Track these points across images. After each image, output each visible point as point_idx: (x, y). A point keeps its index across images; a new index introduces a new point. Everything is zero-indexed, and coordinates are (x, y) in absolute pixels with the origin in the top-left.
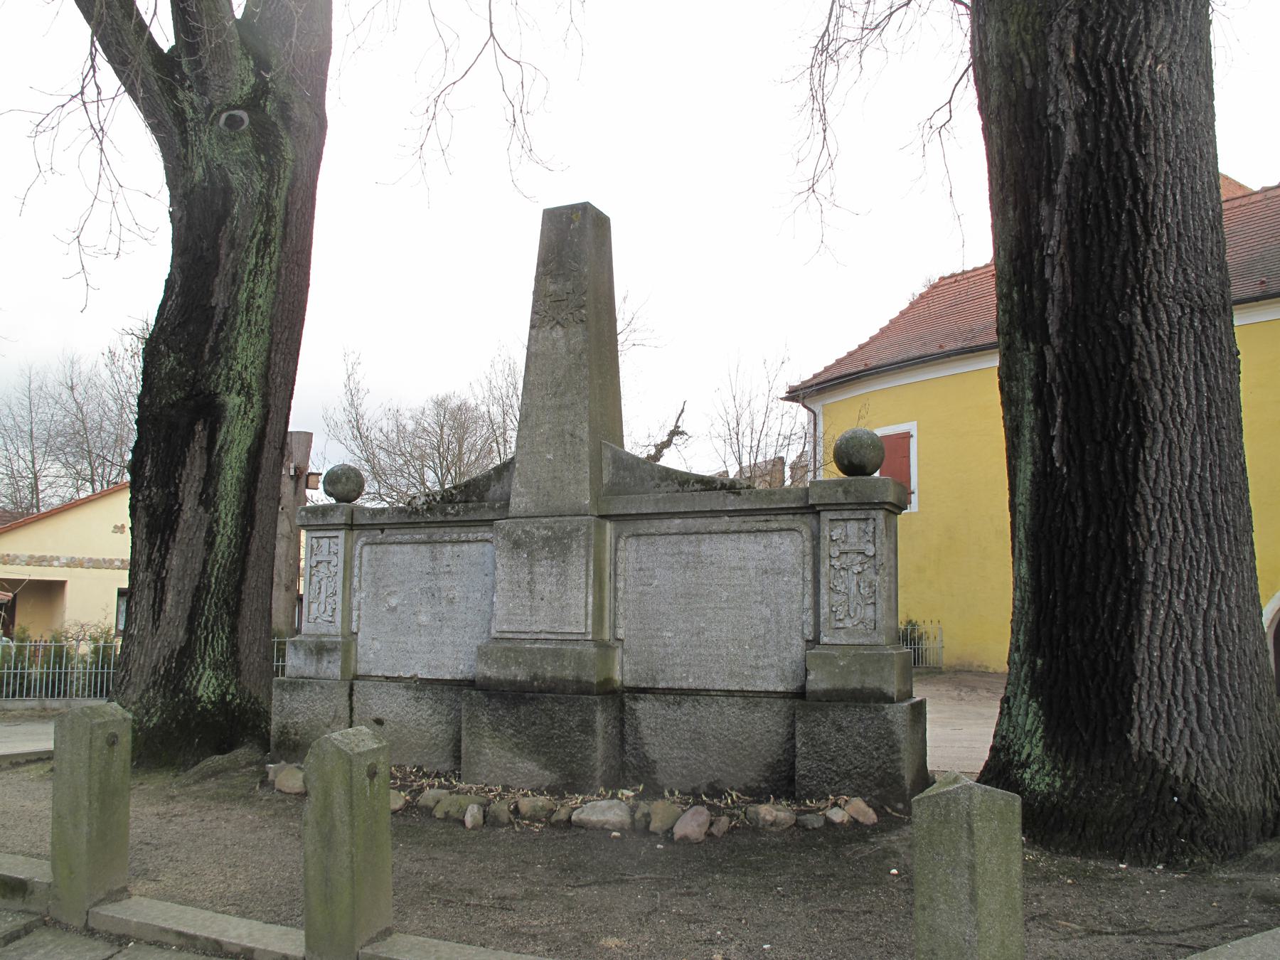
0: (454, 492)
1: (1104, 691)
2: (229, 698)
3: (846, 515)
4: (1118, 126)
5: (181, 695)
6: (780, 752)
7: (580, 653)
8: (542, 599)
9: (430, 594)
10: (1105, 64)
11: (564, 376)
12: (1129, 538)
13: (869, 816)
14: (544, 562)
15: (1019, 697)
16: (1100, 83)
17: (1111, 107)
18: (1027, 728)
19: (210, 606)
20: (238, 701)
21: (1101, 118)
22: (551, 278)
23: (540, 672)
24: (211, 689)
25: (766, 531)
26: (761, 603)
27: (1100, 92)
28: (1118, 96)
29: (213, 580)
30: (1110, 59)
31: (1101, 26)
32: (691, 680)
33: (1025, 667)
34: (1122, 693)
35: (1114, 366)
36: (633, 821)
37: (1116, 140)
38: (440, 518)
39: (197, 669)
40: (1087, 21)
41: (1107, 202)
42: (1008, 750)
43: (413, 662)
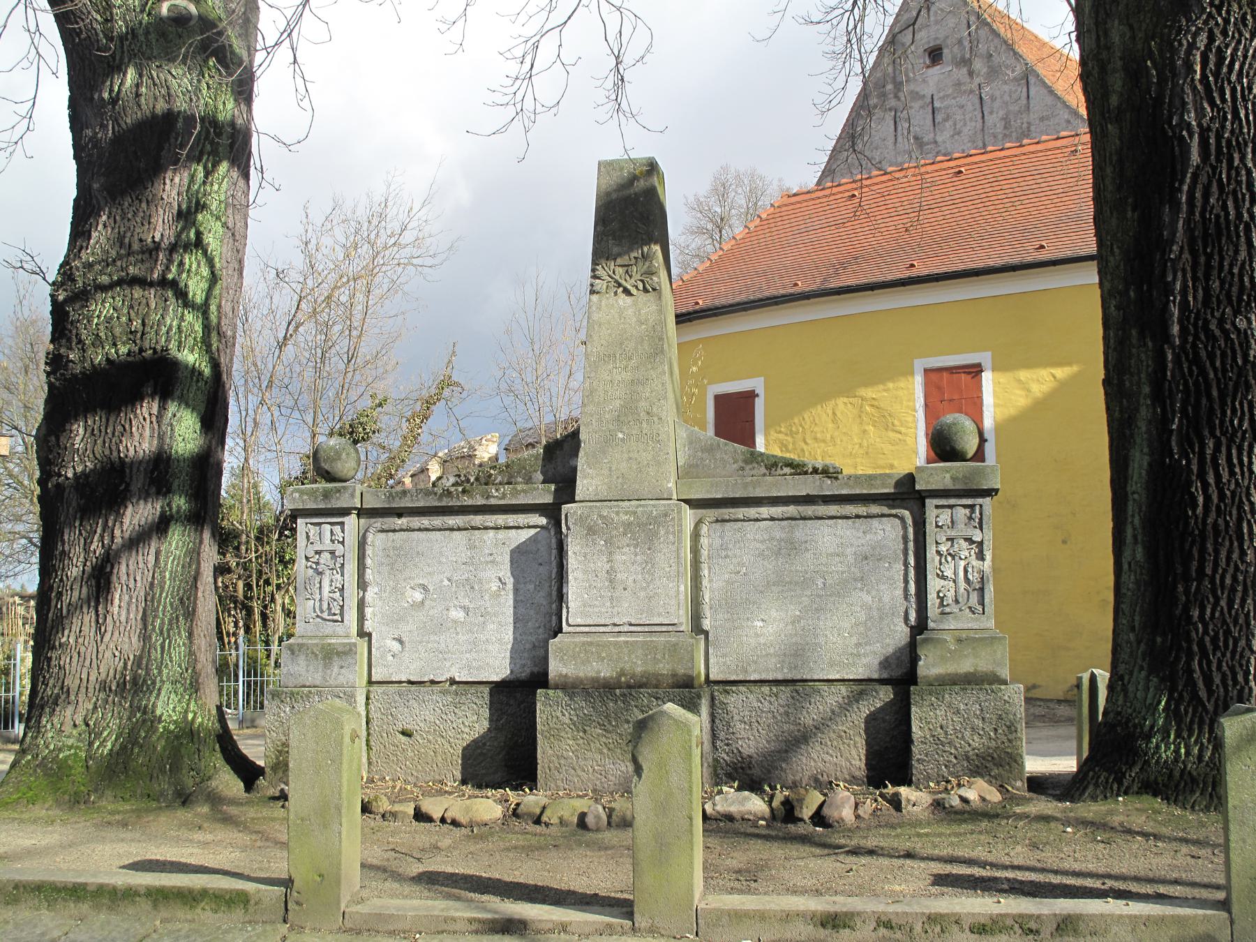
0: (492, 472)
1: (1224, 664)
2: (190, 716)
3: (952, 501)
4: (1237, 140)
5: (138, 715)
6: (888, 739)
7: (675, 645)
8: (625, 589)
9: (468, 587)
10: (1229, 82)
11: (636, 349)
12: (1245, 525)
13: (995, 796)
14: (626, 550)
15: (1135, 673)
16: (1224, 100)
17: (1232, 124)
18: (1148, 702)
19: (165, 607)
20: (200, 720)
21: (1223, 133)
22: (614, 239)
23: (627, 667)
24: (171, 706)
25: (865, 517)
26: (862, 590)
27: (1223, 108)
28: (1239, 114)
29: (167, 574)
30: (1234, 78)
31: (1227, 46)
32: (785, 671)
33: (1143, 647)
34: (1241, 666)
35: (1232, 367)
36: (772, 810)
37: (1236, 156)
38: (480, 501)
39: (154, 683)
40: (1215, 41)
41: (1227, 214)
42: (1127, 723)
43: (448, 664)
